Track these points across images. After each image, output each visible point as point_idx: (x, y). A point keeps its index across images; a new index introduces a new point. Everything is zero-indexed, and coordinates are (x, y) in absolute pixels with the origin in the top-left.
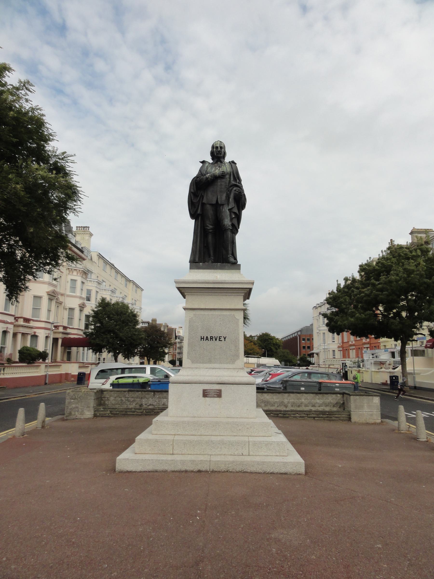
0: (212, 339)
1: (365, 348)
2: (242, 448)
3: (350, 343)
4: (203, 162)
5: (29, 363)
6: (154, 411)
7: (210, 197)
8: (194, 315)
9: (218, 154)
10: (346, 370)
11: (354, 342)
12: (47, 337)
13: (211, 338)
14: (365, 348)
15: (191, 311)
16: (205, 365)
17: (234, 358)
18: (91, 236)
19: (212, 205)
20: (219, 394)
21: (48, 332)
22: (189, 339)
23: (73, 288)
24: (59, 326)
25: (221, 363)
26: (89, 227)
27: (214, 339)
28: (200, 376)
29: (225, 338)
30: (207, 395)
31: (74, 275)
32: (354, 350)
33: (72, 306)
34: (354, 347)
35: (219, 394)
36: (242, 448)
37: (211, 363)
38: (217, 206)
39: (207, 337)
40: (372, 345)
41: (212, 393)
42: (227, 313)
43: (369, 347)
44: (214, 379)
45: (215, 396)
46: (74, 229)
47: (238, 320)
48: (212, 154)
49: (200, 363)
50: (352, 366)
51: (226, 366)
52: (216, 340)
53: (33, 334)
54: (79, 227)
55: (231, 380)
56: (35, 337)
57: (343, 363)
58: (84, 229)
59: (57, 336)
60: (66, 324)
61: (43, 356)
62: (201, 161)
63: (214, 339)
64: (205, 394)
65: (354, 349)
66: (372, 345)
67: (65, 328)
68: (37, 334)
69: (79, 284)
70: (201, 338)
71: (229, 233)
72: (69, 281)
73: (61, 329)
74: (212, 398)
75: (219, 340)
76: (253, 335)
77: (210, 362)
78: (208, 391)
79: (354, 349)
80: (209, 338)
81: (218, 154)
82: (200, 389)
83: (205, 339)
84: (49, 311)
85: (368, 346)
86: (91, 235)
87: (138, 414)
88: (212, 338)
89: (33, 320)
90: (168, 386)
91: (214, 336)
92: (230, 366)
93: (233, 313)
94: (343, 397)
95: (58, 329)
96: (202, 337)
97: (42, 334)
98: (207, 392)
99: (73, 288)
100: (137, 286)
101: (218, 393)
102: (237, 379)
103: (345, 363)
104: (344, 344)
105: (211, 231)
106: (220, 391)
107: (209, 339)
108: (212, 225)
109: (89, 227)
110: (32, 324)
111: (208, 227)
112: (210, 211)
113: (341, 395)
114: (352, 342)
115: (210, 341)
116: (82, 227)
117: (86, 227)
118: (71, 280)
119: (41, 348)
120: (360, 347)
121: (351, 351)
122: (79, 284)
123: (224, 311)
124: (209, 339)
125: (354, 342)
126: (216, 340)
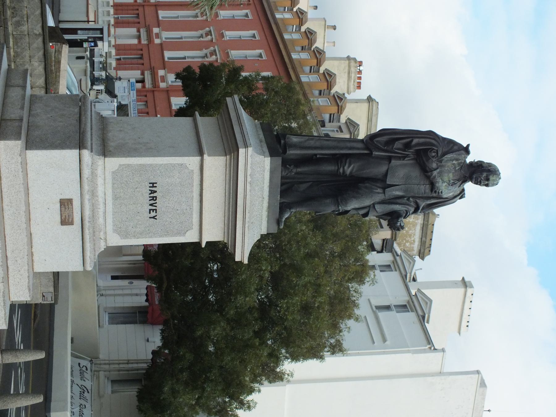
0: (153, 199)
3: (156, 30)
8: (192, 171)
9: (483, 173)
10: (85, 45)
11: (157, 41)
13: (153, 197)
14: (143, 74)
16: (110, 191)
20: (66, 221)
22: (151, 165)
25: (114, 213)
27: (152, 202)
29: (154, 217)
30: (64, 205)
34: (144, 41)
35: (66, 221)
37: (113, 199)
39: (156, 192)
43: (144, 87)
45: (63, 217)
50: (96, 59)
52: (151, 205)
57: (101, 30)
62: (470, 148)
63: (152, 202)
64: (65, 204)
65: (140, 41)
66: (150, 95)
70: (153, 184)
74: (59, 212)
75: (150, 210)
78: (70, 206)
79: (140, 41)
80: (155, 195)
81: (483, 173)
83: (151, 189)
85: (148, 84)
88: (154, 198)
90: (75, 148)
96: (155, 185)
101: (68, 220)
103: (101, 39)
104: (153, 8)
105: (341, 170)
106: (72, 223)
107: (152, 195)
108: (351, 173)
111: (349, 167)
115: (148, 196)
120: (146, 60)
121: (133, 31)
123: (198, 217)
124: (152, 195)
126: (151, 205)
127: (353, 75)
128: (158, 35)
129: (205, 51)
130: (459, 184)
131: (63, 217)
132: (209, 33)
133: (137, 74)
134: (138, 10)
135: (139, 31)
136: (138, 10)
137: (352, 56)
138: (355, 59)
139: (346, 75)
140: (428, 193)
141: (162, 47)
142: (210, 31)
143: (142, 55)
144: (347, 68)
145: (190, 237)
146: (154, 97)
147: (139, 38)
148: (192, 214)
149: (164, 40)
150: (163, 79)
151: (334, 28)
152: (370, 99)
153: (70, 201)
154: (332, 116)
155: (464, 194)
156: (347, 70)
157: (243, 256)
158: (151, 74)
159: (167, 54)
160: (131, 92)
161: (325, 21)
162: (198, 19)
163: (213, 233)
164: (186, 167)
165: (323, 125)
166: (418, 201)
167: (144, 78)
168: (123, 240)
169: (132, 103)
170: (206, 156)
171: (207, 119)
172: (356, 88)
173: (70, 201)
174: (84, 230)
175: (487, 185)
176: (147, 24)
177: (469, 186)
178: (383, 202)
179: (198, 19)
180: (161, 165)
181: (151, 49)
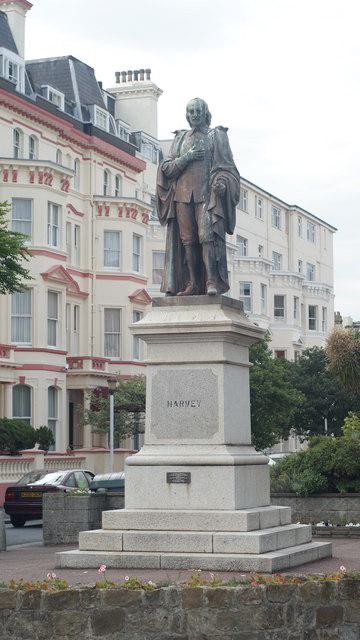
5: (12, 453)
7: (184, 191)
12: (53, 390)
18: (158, 95)
20: (186, 479)
21: (54, 375)
23: (113, 256)
24: (82, 359)
26: (149, 72)
31: (113, 219)
33: (113, 303)
35: (186, 479)
38: (193, 206)
42: (202, 367)
44: (181, 459)
46: (108, 82)
51: (200, 441)
53: (18, 382)
54: (124, 74)
55: (203, 459)
56: (23, 390)
58: (136, 79)
59: (78, 384)
60: (100, 353)
61: (45, 438)
64: (171, 478)
67: (98, 363)
68: (26, 382)
69: (127, 242)
72: (101, 236)
73: (88, 367)
77: (180, 436)
84: (52, 323)
86: (158, 92)
89: (17, 350)
93: (210, 366)
95: (80, 366)
97: (40, 383)
99: (113, 256)
100: (315, 221)
109: (149, 72)
110: (13, 358)
112: (183, 217)
116: (130, 72)
117: (142, 71)
118: (106, 232)
119: (39, 420)
122: (127, 242)
153: (168, 474)
173: (168, 474)
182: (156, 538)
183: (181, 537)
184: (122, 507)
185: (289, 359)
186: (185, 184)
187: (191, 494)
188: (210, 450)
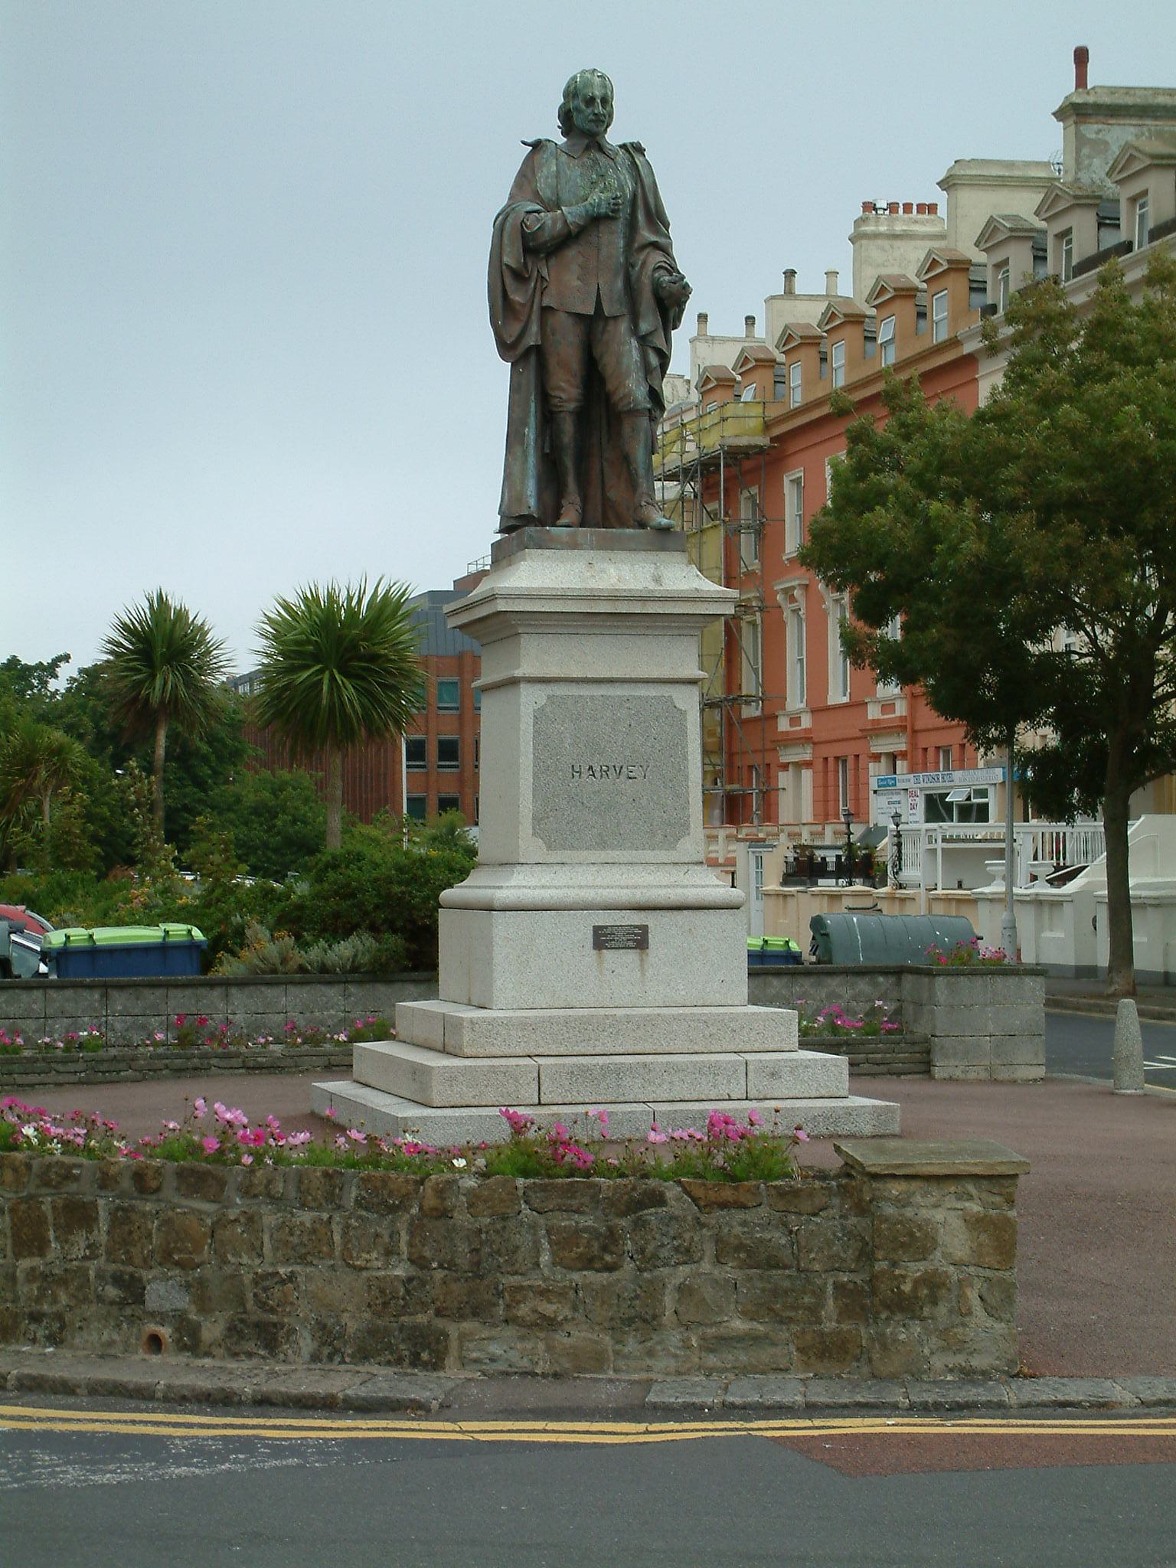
1: (876, 757)
2: (729, 1082)
4: (537, 146)
6: (133, 1064)
8: (549, 697)
9: (585, 113)
11: (806, 722)
14: (876, 757)
15: (539, 686)
17: (671, 833)
19: (579, 317)
20: (640, 940)
22: (535, 776)
28: (581, 887)
30: (607, 941)
32: (807, 775)
34: (806, 754)
35: (640, 940)
36: (729, 1082)
38: (592, 325)
40: (924, 741)
41: (621, 936)
42: (652, 691)
43: (903, 755)
44: (624, 896)
45: (631, 944)
47: (683, 713)
48: (567, 118)
49: (572, 848)
51: (648, 855)
55: (674, 895)
64: (602, 939)
65: (808, 764)
66: (924, 741)
71: (644, 421)
76: (28, 659)
77: (602, 844)
79: (808, 764)
81: (585, 113)
82: (583, 926)
85: (899, 744)
87: (61, 1079)
91: (611, 765)
92: (662, 855)
94: (899, 983)
98: (605, 935)
102: (692, 895)
106: (645, 929)
112: (567, 348)
113: (892, 980)
114: (795, 720)
120: (848, 749)
125: (806, 722)
127: (899, 228)
128: (795, 720)
129: (787, 615)
130: (602, 160)
131: (631, 944)
132: (788, 592)
133: (876, 772)
134: (925, 750)
135: (785, 767)
136: (925, 750)
137: (851, 230)
138: (858, 223)
139: (897, 243)
140: (619, 227)
141: (819, 710)
142: (786, 591)
143: (837, 758)
144: (879, 242)
145: (689, 702)
146: (929, 730)
147: (800, 765)
148: (640, 697)
149: (803, 705)
150: (888, 706)
151: (790, 274)
152: (947, 184)
153: (597, 930)
154: (975, 285)
155: (632, 144)
156: (886, 243)
157: (724, 600)
158: (877, 736)
159: (837, 696)
160: (900, 786)
161: (773, 298)
162: (759, 621)
163: (684, 659)
164: (542, 709)
165: (993, 309)
166: (636, 245)
167: (887, 754)
168: (692, 831)
169: (922, 785)
170: (518, 673)
171: (484, 666)
172: (932, 217)
173: (597, 930)
174: (652, 902)
175: (606, 101)
176: (859, 734)
177: (614, 137)
178: (635, 318)
179: (759, 621)
180: (536, 758)
181: (824, 736)
182: (619, 1072)
183: (677, 1069)
184: (432, 993)
185: (1129, 1001)
186: (575, 268)
187: (649, 973)
188: (677, 876)
